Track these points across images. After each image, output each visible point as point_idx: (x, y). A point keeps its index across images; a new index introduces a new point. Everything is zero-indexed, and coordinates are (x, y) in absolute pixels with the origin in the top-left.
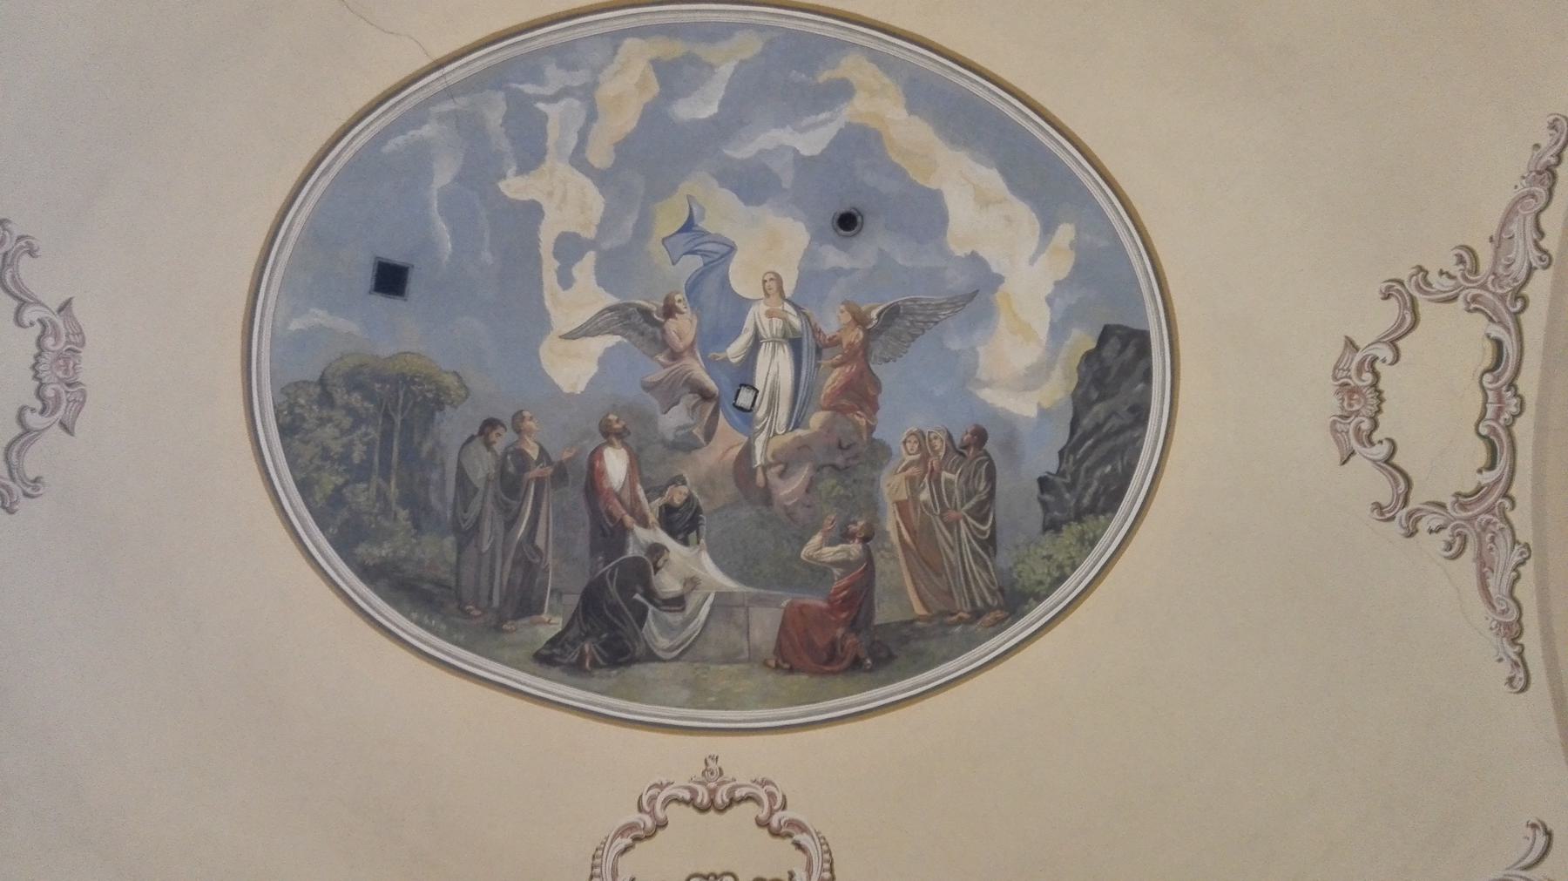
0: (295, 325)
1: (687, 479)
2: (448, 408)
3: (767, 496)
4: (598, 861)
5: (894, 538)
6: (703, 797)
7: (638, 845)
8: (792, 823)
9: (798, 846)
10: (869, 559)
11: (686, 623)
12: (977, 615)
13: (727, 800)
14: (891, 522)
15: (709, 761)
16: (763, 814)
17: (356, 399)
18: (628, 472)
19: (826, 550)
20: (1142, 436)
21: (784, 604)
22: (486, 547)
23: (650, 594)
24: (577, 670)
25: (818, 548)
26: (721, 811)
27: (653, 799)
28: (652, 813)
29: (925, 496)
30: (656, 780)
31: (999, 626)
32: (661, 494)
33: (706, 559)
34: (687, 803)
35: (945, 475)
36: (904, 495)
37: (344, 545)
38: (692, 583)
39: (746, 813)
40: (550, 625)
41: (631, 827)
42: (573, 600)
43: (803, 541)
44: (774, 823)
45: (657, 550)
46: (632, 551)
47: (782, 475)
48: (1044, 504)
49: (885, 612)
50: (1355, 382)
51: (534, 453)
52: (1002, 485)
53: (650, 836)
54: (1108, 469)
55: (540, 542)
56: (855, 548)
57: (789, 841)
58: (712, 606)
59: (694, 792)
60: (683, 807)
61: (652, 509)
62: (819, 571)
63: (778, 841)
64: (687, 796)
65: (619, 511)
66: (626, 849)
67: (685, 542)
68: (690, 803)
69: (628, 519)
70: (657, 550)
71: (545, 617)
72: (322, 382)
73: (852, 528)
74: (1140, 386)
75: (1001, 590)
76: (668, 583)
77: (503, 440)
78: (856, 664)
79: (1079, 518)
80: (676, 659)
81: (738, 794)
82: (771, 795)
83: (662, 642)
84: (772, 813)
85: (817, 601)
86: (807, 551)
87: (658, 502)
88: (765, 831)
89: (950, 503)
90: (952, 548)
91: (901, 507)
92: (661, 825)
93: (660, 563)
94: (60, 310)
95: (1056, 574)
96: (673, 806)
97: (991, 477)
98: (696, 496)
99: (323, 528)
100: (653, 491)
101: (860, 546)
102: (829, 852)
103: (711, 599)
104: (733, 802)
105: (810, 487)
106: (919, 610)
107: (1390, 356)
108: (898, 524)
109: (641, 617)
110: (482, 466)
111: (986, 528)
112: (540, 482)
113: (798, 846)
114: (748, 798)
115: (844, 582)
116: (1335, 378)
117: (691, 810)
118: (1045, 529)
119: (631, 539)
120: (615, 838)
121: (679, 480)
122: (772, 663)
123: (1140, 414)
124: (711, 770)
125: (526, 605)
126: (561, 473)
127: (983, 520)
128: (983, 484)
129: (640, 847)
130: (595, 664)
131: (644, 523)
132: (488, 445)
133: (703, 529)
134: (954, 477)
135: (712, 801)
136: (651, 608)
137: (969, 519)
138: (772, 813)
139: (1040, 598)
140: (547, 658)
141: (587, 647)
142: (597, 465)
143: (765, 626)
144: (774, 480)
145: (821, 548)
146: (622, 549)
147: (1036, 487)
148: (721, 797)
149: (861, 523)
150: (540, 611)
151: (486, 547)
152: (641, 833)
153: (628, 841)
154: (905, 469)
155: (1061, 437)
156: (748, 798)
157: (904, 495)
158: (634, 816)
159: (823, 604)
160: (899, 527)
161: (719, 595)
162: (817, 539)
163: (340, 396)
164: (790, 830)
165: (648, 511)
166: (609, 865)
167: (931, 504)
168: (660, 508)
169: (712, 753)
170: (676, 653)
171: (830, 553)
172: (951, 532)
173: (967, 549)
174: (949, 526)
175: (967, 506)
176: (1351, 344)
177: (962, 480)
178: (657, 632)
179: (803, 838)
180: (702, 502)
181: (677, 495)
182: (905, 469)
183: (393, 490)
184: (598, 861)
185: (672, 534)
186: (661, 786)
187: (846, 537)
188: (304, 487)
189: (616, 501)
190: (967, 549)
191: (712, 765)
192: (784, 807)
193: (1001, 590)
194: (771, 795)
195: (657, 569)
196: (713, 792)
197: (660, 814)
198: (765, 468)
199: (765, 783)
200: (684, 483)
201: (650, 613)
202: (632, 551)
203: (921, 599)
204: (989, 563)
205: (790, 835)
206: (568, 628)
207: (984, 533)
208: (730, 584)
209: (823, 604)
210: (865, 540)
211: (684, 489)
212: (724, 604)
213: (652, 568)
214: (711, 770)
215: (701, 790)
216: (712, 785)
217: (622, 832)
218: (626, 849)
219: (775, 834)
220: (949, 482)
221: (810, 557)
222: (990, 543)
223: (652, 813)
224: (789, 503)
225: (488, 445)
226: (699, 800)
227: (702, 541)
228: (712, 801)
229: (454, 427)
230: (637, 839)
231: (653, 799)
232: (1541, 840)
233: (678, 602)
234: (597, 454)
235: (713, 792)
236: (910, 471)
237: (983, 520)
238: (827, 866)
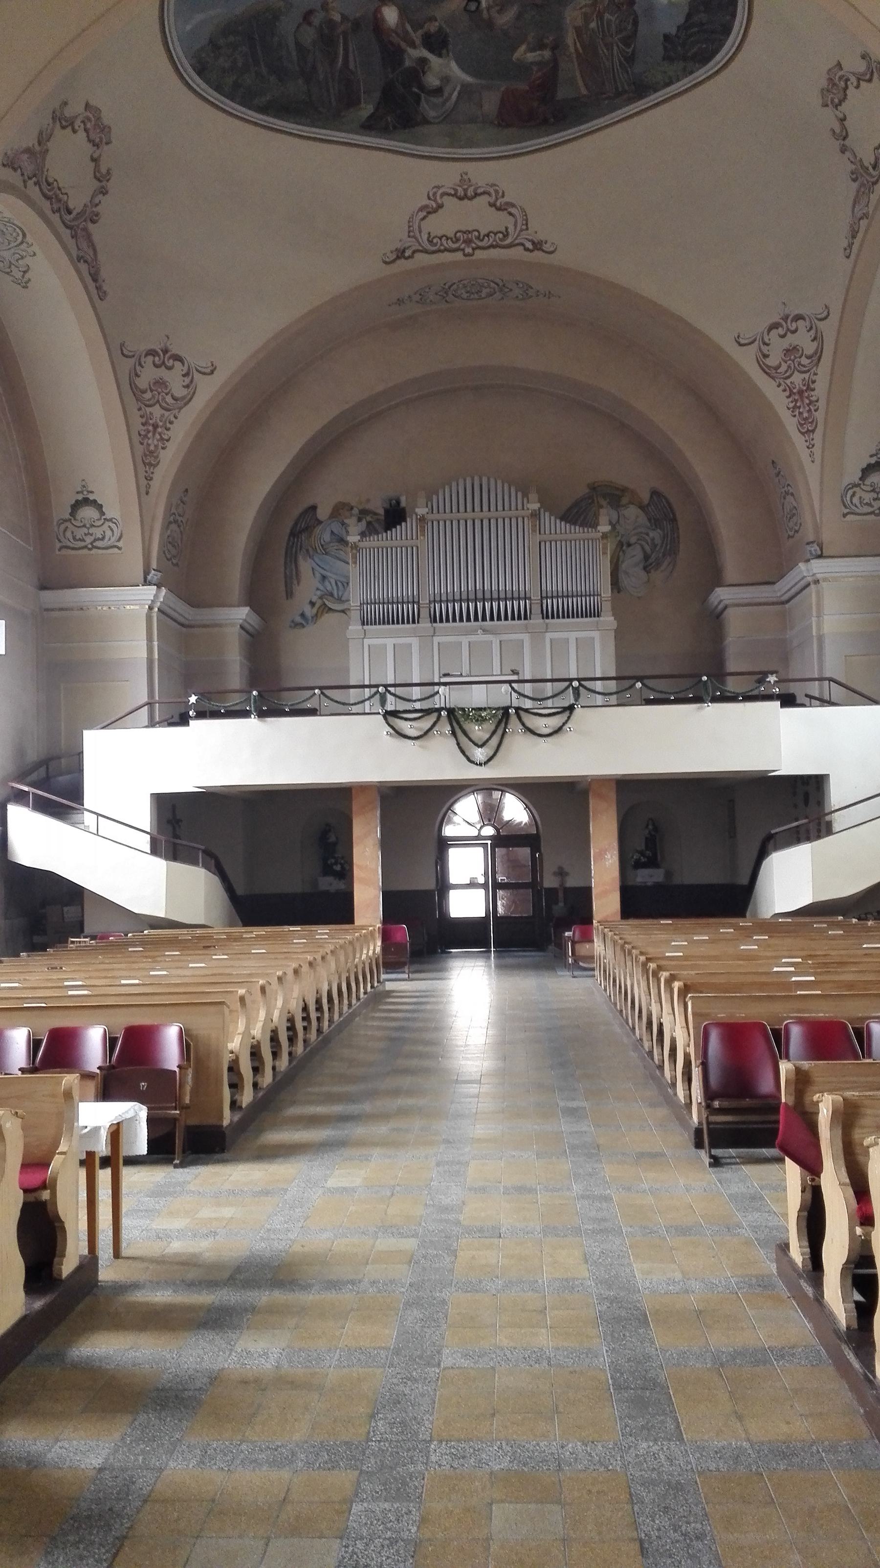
0: (188, 27)
1: (438, 17)
2: (282, 18)
3: (490, 24)
4: (411, 224)
5: (572, 49)
6: (461, 192)
7: (430, 216)
8: (507, 204)
9: (510, 214)
10: (555, 61)
11: (444, 103)
12: (618, 94)
13: (473, 194)
14: (570, 39)
15: (464, 175)
16: (492, 200)
17: (231, 39)
18: (399, 17)
19: (529, 55)
20: (726, 40)
21: (503, 89)
22: (321, 77)
23: (422, 87)
24: (385, 131)
25: (523, 54)
26: (471, 199)
27: (435, 194)
28: (435, 200)
29: (593, 25)
30: (437, 184)
31: (630, 101)
32: (422, 27)
33: (453, 65)
34: (452, 195)
35: (607, 16)
36: (579, 22)
37: (247, 102)
38: (446, 80)
39: (483, 200)
40: (366, 110)
41: (426, 206)
42: (377, 95)
43: (514, 49)
44: (498, 204)
45: (423, 61)
46: (408, 63)
47: (500, 12)
48: (665, 48)
49: (563, 93)
50: (836, 81)
51: (337, 17)
52: (642, 28)
53: (435, 211)
54: (704, 46)
55: (352, 66)
56: (547, 54)
57: (505, 212)
58: (459, 94)
59: (456, 190)
60: (451, 197)
61: (417, 37)
62: (523, 68)
63: (501, 213)
64: (453, 192)
65: (395, 40)
66: (424, 218)
67: (440, 55)
68: (455, 195)
69: (403, 45)
70: (423, 61)
71: (363, 105)
72: (211, 41)
73: (546, 41)
74: (728, 18)
75: (634, 83)
76: (432, 80)
77: (317, 20)
78: (545, 121)
79: (685, 59)
80: (439, 123)
81: (479, 191)
82: (497, 192)
83: (432, 114)
84: (497, 199)
85: (523, 86)
86: (517, 55)
87: (420, 32)
88: (493, 209)
89: (609, 32)
90: (608, 59)
91: (578, 31)
92: (440, 206)
93: (426, 68)
94: (86, 110)
95: (667, 81)
96: (445, 197)
97: (636, 23)
98: (444, 26)
99: (232, 100)
100: (417, 26)
101: (550, 53)
102: (526, 215)
103: (458, 89)
104: (476, 195)
105: (519, 16)
106: (584, 91)
107: (855, 84)
108: (575, 40)
109: (418, 100)
110: (309, 35)
111: (630, 50)
112: (345, 34)
113: (510, 214)
114: (484, 193)
115: (540, 74)
116: (828, 73)
117: (455, 200)
118: (664, 59)
119: (406, 56)
120: (418, 212)
121: (433, 19)
122: (496, 122)
123: (727, 30)
124: (464, 180)
125: (350, 100)
126: (357, 25)
127: (628, 46)
128: (630, 27)
129: (431, 216)
130: (395, 128)
131: (413, 45)
132: (310, 24)
133: (450, 47)
134: (613, 19)
135: (466, 195)
136: (422, 95)
137: (620, 44)
138: (497, 199)
139: (656, 90)
140: (369, 126)
141: (389, 119)
142: (379, 16)
143: (491, 103)
144: (494, 12)
145: (525, 54)
146: (401, 62)
147: (662, 38)
148: (470, 192)
149: (551, 38)
150: (359, 102)
151: (321, 77)
152: (431, 210)
153: (425, 214)
154: (581, 8)
155: (681, 20)
156: (484, 193)
157: (579, 22)
158: (427, 202)
159: (527, 88)
160: (575, 44)
161: (463, 86)
162: (523, 48)
163: (222, 42)
164: (506, 207)
165: (415, 38)
166: (417, 224)
167: (596, 29)
168: (422, 36)
169: (465, 170)
170: (441, 118)
171: (531, 57)
172: (608, 49)
173: (616, 60)
174: (606, 45)
175: (619, 36)
176: (839, 65)
177: (617, 22)
178: (428, 109)
179: (513, 210)
180: (448, 30)
181: (433, 27)
182: (581, 8)
183: (264, 70)
184: (411, 224)
185: (431, 50)
186: (438, 187)
187: (541, 46)
188: (218, 89)
189: (394, 35)
190: (616, 60)
191: (465, 177)
192: (503, 196)
193: (634, 83)
194: (497, 192)
195: (424, 73)
196: (465, 190)
197: (440, 201)
198: (489, 8)
199: (493, 185)
200: (436, 20)
201: (423, 99)
202: (408, 63)
203: (586, 85)
204: (629, 69)
205: (506, 209)
206: (377, 109)
207: (627, 53)
208: (469, 79)
209: (527, 88)
210: (554, 48)
211: (437, 24)
212: (466, 91)
213: (421, 72)
214: (464, 180)
215: (460, 190)
216: (465, 187)
217: (421, 209)
218: (424, 218)
219: (499, 209)
220: (609, 21)
221: (518, 59)
222: (631, 59)
223: (435, 200)
224: (506, 27)
225: (310, 24)
226: (459, 194)
227: (451, 54)
228: (466, 195)
229: (288, 25)
230: (429, 213)
231: (435, 194)
232: (825, 313)
233: (439, 91)
234: (378, 11)
235: (465, 190)
236: (583, 10)
237: (628, 46)
238: (524, 222)
